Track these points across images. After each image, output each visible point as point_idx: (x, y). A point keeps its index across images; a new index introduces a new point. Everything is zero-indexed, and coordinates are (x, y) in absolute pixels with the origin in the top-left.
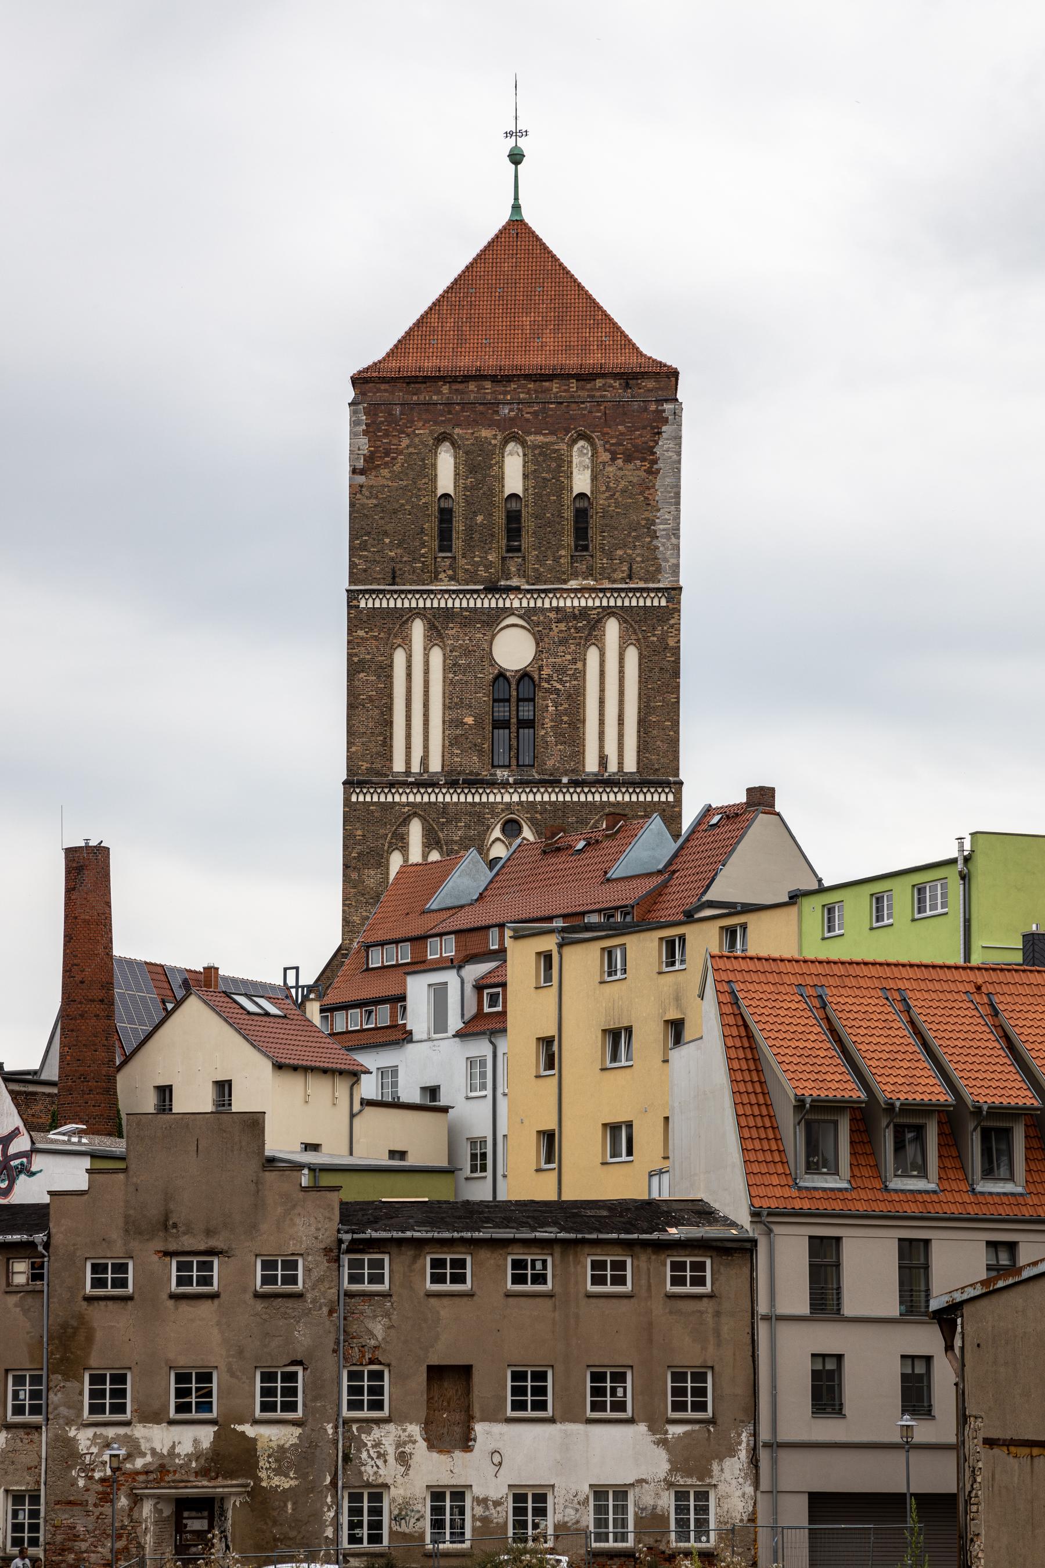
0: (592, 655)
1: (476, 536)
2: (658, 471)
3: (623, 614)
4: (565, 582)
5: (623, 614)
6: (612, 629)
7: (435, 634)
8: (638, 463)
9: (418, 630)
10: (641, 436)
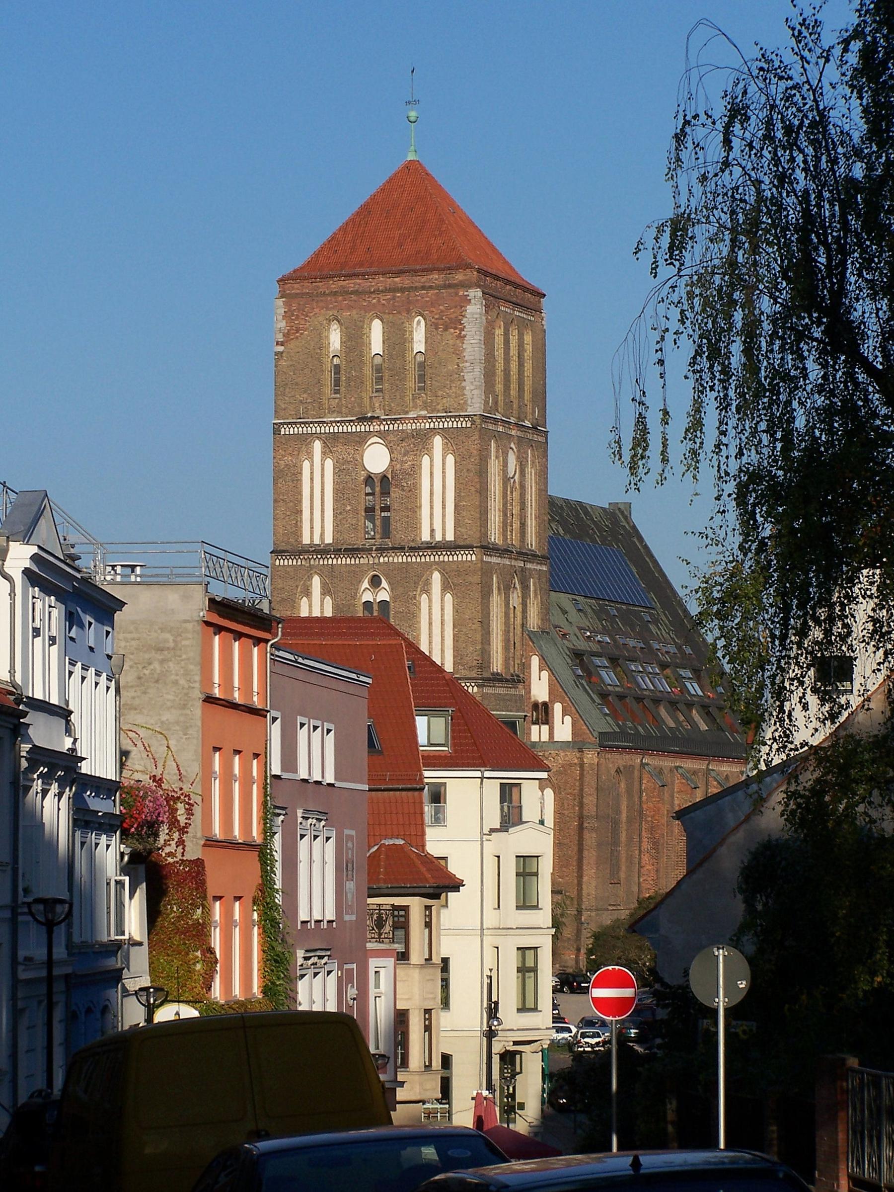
0: (426, 460)
1: (352, 384)
2: (465, 336)
3: (444, 432)
4: (407, 413)
5: (444, 432)
6: (438, 441)
7: (327, 452)
8: (452, 330)
9: (317, 446)
10: (454, 312)
